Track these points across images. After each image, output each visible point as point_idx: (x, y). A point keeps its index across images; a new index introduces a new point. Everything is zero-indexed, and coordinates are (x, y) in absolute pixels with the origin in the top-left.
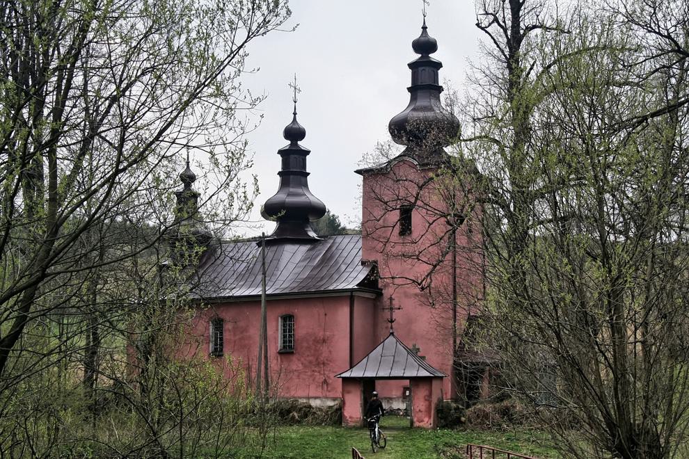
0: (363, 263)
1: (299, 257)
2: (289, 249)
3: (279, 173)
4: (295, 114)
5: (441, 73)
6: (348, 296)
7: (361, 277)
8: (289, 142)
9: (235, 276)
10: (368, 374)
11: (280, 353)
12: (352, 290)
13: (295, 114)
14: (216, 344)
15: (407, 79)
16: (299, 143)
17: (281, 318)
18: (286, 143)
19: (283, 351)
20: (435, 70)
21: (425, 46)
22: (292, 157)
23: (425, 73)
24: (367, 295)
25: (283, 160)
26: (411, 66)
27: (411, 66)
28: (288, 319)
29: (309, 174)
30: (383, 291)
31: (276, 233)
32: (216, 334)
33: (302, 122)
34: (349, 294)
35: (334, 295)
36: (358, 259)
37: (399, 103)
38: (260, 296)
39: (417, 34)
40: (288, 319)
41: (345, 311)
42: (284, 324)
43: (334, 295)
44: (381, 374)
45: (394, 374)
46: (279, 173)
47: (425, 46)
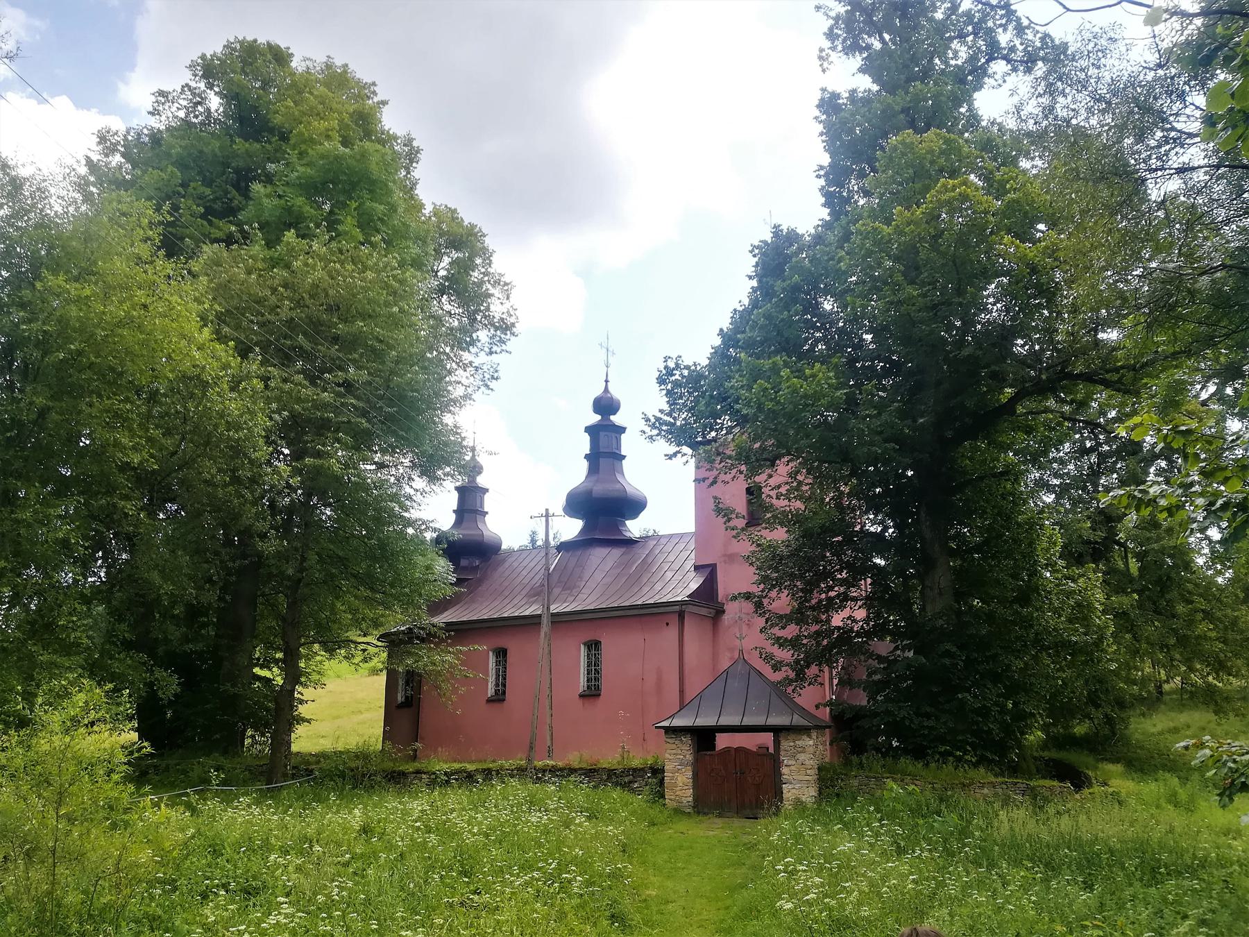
0: (697, 568)
1: (610, 563)
2: (599, 553)
3: (587, 457)
4: (607, 381)
6: (676, 612)
7: (694, 586)
8: (598, 417)
9: (524, 592)
10: (701, 722)
11: (581, 696)
12: (682, 603)
13: (607, 381)
14: (497, 685)
15: (584, 444)
16: (612, 418)
21: (606, 406)
22: (602, 434)
24: (704, 611)
25: (742, 319)
26: (589, 430)
27: (589, 430)
28: (594, 646)
29: (624, 457)
31: (583, 531)
33: (615, 392)
35: (642, 612)
36: (690, 564)
37: (576, 474)
38: (539, 616)
39: (599, 391)
40: (594, 646)
41: (672, 633)
44: (725, 721)
45: (748, 721)
46: (587, 457)
47: (606, 406)
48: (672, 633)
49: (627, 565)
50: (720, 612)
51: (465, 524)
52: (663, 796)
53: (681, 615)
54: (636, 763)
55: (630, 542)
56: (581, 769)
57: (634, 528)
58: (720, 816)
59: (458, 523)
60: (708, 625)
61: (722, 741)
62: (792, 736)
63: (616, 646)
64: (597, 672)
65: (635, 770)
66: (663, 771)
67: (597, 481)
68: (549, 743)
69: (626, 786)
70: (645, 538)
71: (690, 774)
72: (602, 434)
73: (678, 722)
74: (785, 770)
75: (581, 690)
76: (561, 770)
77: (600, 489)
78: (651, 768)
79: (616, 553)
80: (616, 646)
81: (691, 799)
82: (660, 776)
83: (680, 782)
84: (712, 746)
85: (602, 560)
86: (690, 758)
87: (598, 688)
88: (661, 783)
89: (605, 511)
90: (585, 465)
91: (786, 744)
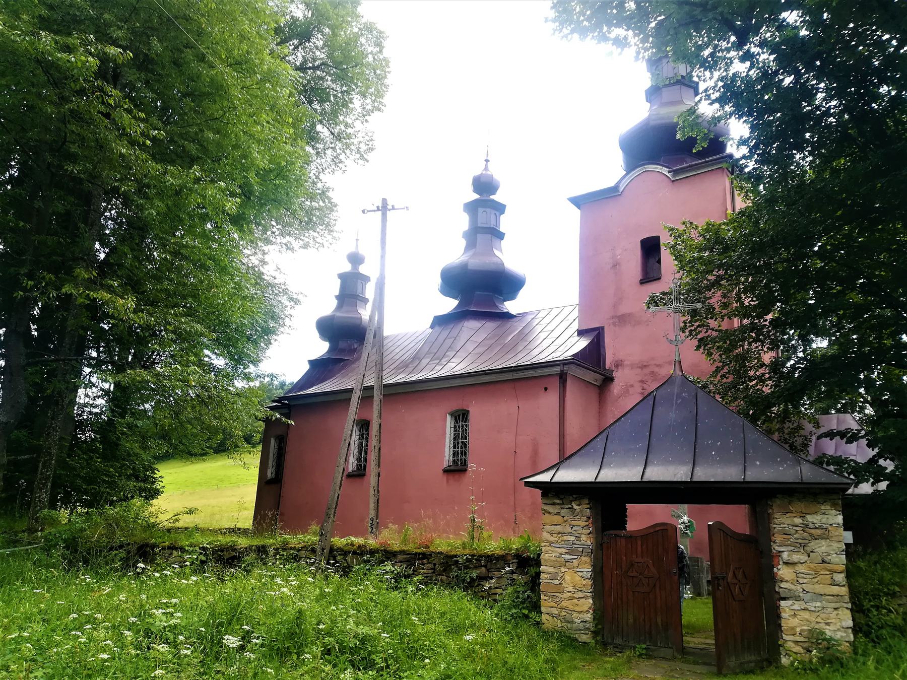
1: (480, 337)
2: (471, 325)
3: (337, 297)
5: (503, 219)
8: (477, 196)
10: (611, 474)
11: (446, 471)
14: (359, 460)
15: (464, 222)
17: (452, 415)
18: (347, 267)
19: (452, 468)
20: (498, 214)
21: (484, 186)
23: (484, 217)
28: (461, 416)
30: (649, 105)
32: (361, 444)
34: (557, 369)
35: (532, 373)
40: (461, 416)
41: (550, 400)
42: (455, 427)
43: (532, 373)
46: (337, 297)
47: (484, 186)
48: (550, 400)
49: (502, 337)
50: (608, 379)
51: (345, 308)
52: (536, 607)
53: (563, 377)
54: (493, 545)
55: (507, 316)
56: (403, 552)
57: (510, 306)
58: (648, 655)
59: (340, 307)
60: (594, 395)
61: (640, 517)
62: (798, 506)
63: (485, 415)
64: (465, 445)
65: (490, 558)
66: (537, 562)
67: (474, 254)
68: (372, 513)
69: (472, 586)
70: (523, 315)
71: (587, 570)
72: (480, 210)
73: (566, 475)
74: (783, 572)
75: (445, 465)
76: (372, 552)
77: (477, 262)
78: (517, 556)
79: (490, 325)
80: (485, 415)
81: (588, 617)
82: (533, 571)
83: (570, 588)
84: (620, 520)
85: (474, 332)
86: (587, 540)
87: (465, 463)
88: (534, 583)
89: (482, 292)
90: (463, 243)
91: (784, 521)
